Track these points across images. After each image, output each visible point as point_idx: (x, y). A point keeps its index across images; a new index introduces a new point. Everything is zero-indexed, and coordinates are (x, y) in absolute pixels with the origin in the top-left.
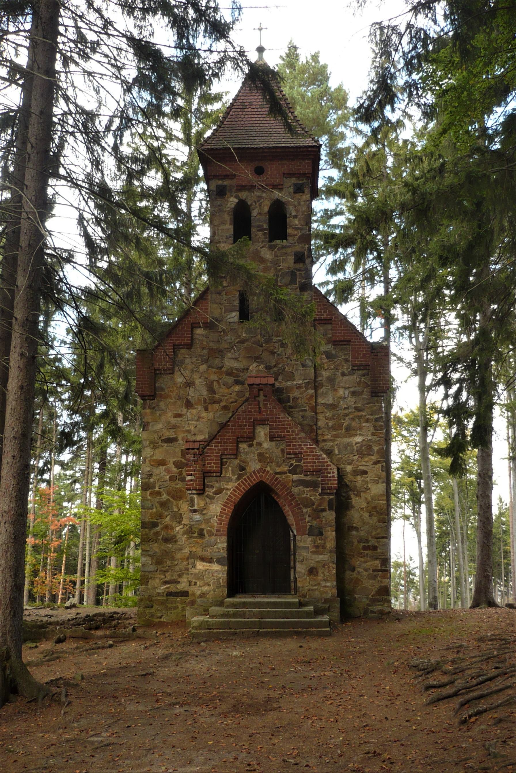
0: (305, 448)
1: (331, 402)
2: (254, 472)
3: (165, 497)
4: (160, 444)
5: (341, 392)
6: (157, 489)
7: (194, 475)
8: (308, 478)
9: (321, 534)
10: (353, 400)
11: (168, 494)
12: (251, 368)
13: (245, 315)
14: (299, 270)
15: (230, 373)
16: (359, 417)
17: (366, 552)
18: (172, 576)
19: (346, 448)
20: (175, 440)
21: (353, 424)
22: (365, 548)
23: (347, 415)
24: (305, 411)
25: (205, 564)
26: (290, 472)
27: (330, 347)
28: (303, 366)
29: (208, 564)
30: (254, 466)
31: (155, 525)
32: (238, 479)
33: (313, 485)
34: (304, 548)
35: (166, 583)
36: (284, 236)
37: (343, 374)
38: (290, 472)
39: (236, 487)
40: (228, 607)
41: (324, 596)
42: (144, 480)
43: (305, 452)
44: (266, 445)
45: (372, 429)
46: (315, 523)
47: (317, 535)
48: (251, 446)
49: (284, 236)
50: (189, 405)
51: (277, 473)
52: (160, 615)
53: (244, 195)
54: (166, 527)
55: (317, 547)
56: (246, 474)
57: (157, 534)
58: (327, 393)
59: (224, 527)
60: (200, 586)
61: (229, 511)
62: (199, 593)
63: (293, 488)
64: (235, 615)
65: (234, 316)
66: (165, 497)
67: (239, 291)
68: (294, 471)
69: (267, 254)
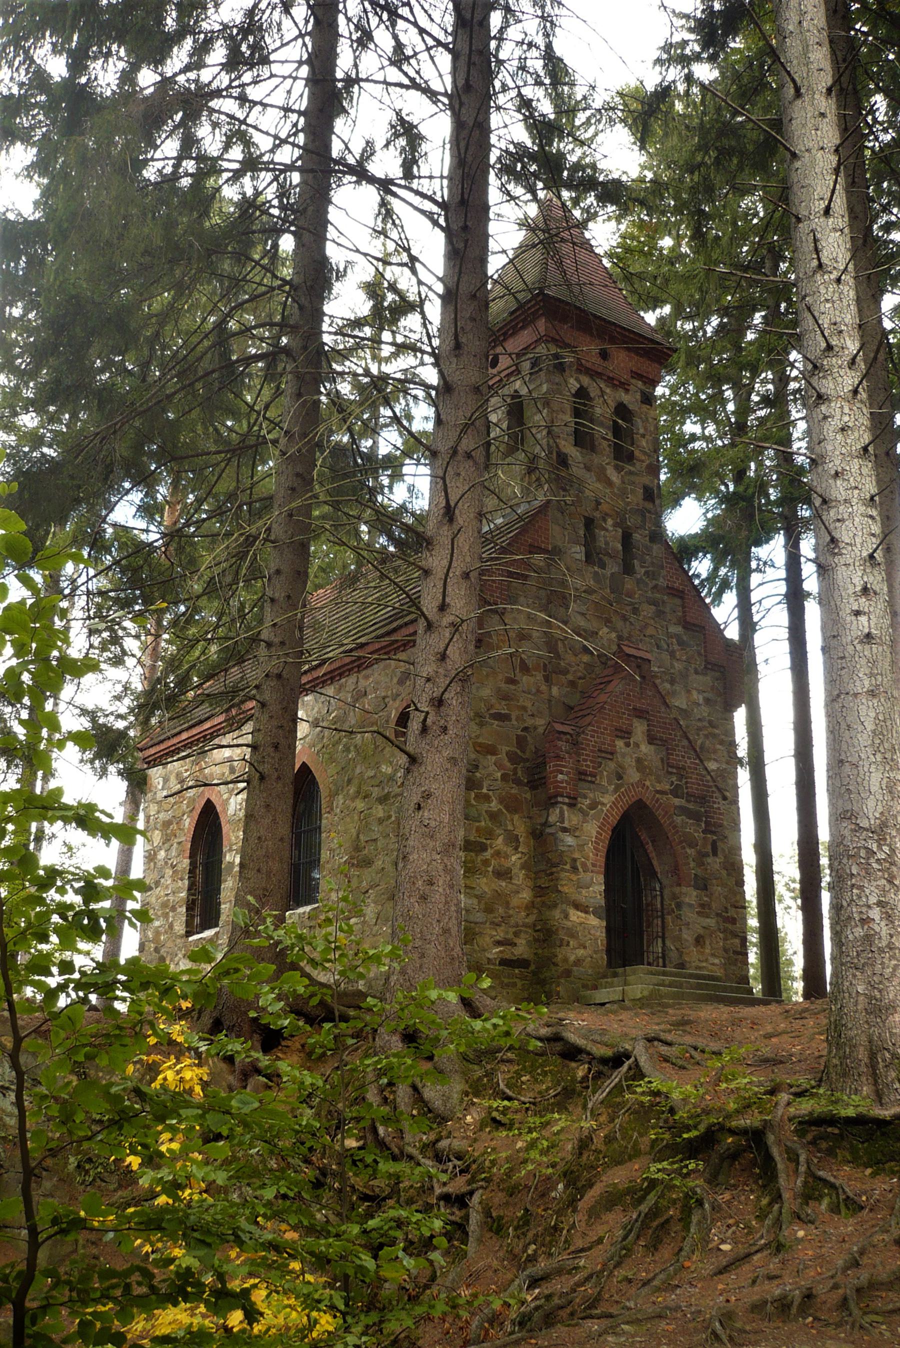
1: (684, 707)
3: (494, 805)
6: (485, 791)
7: (568, 774)
8: (691, 806)
9: (705, 888)
11: (501, 801)
16: (715, 736)
30: (633, 776)
32: (616, 790)
33: (695, 816)
35: (499, 943)
37: (696, 672)
44: (645, 748)
46: (699, 872)
51: (658, 792)
54: (498, 854)
55: (702, 906)
59: (601, 860)
61: (606, 836)
62: (572, 958)
66: (494, 805)
68: (675, 792)
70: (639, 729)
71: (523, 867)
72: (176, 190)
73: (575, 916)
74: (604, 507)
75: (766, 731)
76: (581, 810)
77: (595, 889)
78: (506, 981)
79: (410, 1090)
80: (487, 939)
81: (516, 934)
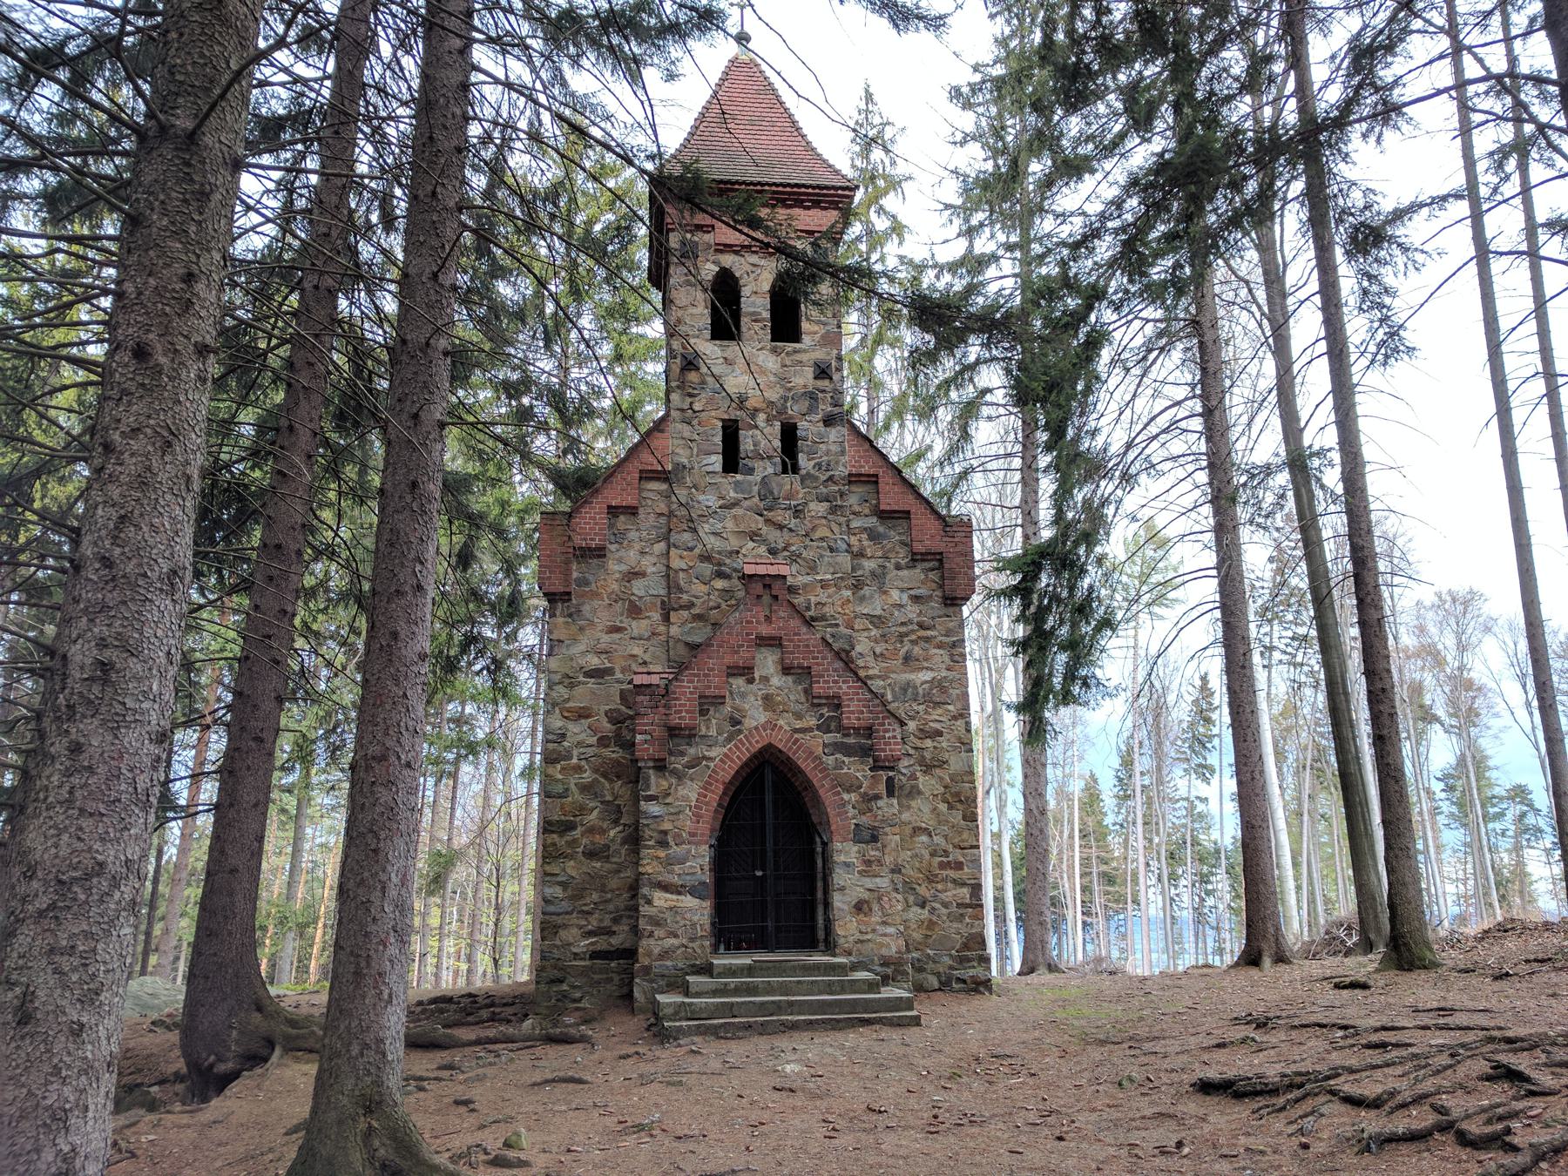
0: (844, 686)
1: (878, 612)
2: (756, 728)
4: (581, 679)
5: (895, 595)
6: (575, 761)
8: (851, 740)
10: (917, 608)
11: (596, 771)
12: (743, 551)
13: (732, 462)
14: (823, 391)
15: (706, 558)
16: (927, 639)
17: (944, 873)
18: (601, 920)
19: (905, 691)
20: (608, 672)
21: (917, 650)
22: (942, 866)
23: (907, 635)
24: (837, 625)
25: (669, 896)
26: (819, 728)
27: (873, 521)
28: (832, 550)
29: (674, 897)
30: (756, 716)
31: (571, 826)
34: (847, 865)
35: (590, 934)
36: (796, 337)
37: (898, 567)
38: (819, 728)
39: (726, 755)
40: (720, 975)
41: (884, 952)
42: (551, 746)
43: (846, 694)
44: (776, 681)
45: (947, 659)
46: (865, 820)
47: (867, 842)
48: (751, 681)
49: (796, 337)
50: (635, 611)
51: (796, 731)
52: (578, 995)
53: (728, 260)
56: (740, 732)
57: (573, 843)
58: (872, 597)
60: (660, 939)
62: (656, 951)
63: (825, 758)
64: (737, 991)
65: (716, 461)
67: (723, 420)
68: (824, 728)
69: (769, 362)
70: (767, 663)
71: (624, 843)
72: (1001, 175)
73: (661, 899)
74: (750, 404)
75: (1532, 528)
76: (674, 772)
77: (698, 861)
78: (596, 977)
79: (1537, 805)
80: (575, 931)
81: (616, 921)
